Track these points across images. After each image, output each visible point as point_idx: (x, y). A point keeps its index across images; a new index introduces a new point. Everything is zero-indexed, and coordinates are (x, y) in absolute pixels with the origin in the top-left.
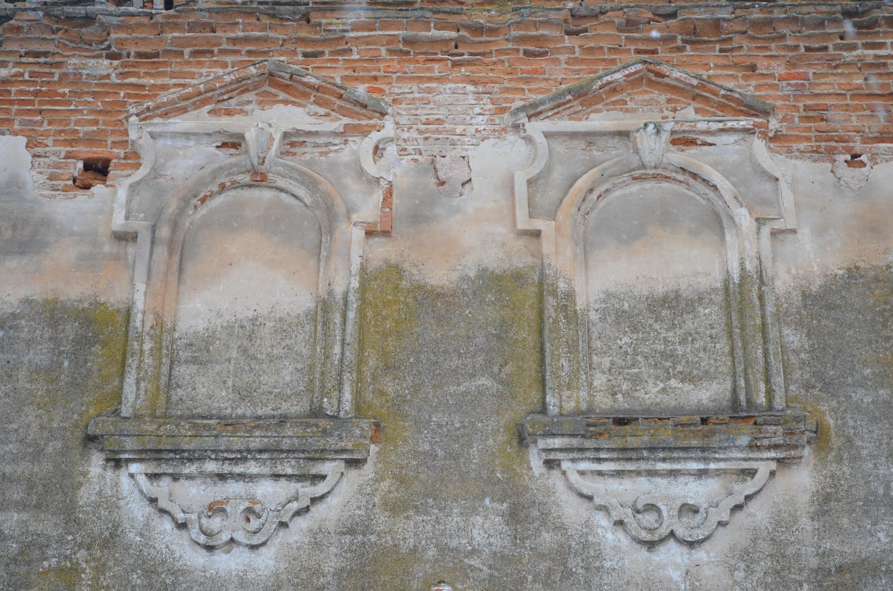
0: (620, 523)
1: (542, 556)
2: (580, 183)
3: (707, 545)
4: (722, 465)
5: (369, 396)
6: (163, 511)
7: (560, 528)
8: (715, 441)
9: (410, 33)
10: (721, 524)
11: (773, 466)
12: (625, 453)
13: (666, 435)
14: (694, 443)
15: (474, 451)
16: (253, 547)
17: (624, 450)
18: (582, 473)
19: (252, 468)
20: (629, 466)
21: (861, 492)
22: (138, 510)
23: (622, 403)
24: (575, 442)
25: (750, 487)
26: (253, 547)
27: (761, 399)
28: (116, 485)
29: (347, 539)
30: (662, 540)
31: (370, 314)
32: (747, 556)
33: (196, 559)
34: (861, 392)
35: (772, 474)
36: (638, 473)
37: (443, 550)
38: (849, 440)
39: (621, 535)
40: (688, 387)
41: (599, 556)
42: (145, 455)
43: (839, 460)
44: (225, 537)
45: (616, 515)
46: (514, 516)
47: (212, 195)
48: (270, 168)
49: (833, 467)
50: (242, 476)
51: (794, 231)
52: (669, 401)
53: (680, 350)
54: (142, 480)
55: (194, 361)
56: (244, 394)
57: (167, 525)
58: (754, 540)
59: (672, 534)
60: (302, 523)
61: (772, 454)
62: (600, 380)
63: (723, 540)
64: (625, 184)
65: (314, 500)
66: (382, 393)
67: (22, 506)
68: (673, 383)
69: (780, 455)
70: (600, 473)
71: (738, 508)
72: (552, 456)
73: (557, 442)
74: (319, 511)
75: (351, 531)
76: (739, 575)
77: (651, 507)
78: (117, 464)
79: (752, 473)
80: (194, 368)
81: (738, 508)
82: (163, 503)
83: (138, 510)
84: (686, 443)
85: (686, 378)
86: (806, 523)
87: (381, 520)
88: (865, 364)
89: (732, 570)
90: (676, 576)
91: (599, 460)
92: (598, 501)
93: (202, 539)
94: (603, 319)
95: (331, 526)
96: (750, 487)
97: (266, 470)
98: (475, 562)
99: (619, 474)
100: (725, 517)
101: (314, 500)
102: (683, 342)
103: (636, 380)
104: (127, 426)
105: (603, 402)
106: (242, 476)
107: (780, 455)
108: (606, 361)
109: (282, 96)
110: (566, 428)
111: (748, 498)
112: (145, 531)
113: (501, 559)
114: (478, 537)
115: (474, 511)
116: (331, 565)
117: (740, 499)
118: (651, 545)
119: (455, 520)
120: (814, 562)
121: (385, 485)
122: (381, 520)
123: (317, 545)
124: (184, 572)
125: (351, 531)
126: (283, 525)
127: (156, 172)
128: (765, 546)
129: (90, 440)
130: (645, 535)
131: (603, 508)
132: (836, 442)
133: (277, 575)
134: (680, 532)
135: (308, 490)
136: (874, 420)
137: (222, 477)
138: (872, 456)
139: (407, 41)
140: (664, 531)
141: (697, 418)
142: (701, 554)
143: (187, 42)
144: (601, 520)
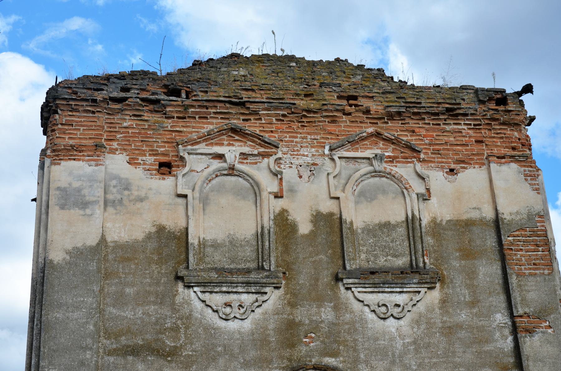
11: (426, 289)
12: (375, 285)
13: (389, 278)
18: (359, 292)
19: (240, 289)
20: (376, 290)
26: (242, 319)
29: (276, 317)
35: (426, 292)
36: (379, 292)
40: (395, 259)
44: (232, 316)
47: (213, 179)
50: (236, 292)
52: (388, 265)
56: (233, 260)
58: (420, 317)
73: (351, 281)
74: (265, 306)
75: (277, 314)
76: (415, 330)
83: (199, 305)
89: (413, 328)
90: (393, 330)
92: (365, 303)
96: (418, 297)
97: (244, 290)
98: (323, 325)
103: (376, 256)
105: (365, 265)
108: (365, 249)
120: (440, 325)
126: (253, 311)
131: (368, 306)
142: (401, 322)
143: (197, 113)
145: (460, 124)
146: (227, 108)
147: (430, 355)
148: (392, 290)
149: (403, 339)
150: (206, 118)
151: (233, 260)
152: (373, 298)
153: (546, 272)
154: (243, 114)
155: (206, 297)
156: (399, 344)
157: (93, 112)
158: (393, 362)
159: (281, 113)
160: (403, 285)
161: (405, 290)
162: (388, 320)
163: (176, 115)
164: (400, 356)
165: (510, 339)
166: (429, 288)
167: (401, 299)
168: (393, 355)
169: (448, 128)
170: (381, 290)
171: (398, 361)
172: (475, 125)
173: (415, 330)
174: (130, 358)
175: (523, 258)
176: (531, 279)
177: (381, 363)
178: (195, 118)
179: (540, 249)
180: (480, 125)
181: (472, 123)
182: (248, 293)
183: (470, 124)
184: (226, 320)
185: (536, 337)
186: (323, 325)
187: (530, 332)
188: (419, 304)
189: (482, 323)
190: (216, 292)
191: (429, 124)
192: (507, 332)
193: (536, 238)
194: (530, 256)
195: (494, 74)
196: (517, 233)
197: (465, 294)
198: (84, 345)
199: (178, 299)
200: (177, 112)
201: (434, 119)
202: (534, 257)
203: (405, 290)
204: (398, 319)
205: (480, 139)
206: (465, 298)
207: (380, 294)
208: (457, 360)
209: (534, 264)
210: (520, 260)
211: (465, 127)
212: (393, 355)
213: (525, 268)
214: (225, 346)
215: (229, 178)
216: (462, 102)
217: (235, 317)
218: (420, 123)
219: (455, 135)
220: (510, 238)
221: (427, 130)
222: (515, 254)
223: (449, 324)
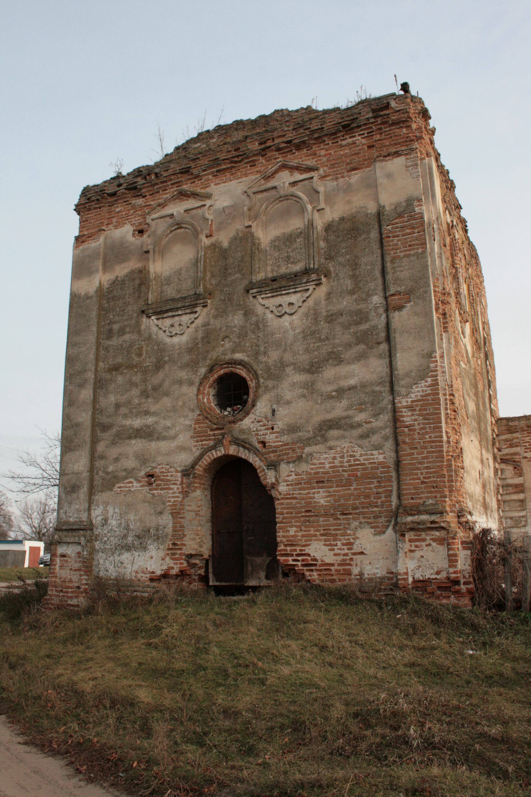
0: (272, 312)
1: (252, 324)
2: (263, 207)
3: (296, 314)
4: (300, 289)
5: (208, 286)
6: (160, 328)
7: (257, 316)
8: (297, 282)
9: (218, 169)
10: (300, 307)
11: (314, 286)
12: (272, 290)
13: (284, 283)
14: (291, 284)
15: (235, 297)
16: (181, 334)
17: (272, 289)
18: (262, 298)
19: (180, 312)
20: (275, 294)
21: (339, 290)
22: (154, 329)
23: (275, 274)
24: (259, 290)
25: (307, 294)
26: (181, 334)
27: (312, 266)
28: (149, 323)
29: (204, 328)
30: (283, 315)
31: (208, 261)
32: (306, 315)
33: (168, 340)
34: (341, 258)
35: (314, 289)
36: (277, 295)
37: (227, 327)
38: (337, 274)
39: (273, 315)
40: (293, 266)
41: (267, 322)
42: (156, 313)
43: (334, 281)
44: (174, 333)
45: (271, 309)
46: (246, 314)
47: (168, 234)
48: (392, 511)
49: (332, 283)
50: (178, 315)
51: (323, 209)
52: (288, 271)
53: (291, 254)
54: (155, 321)
55: (167, 284)
56: (179, 291)
57: (161, 332)
58: (309, 310)
59: (286, 312)
60: (193, 325)
61: (313, 283)
62: (269, 268)
63: (301, 311)
64: (277, 204)
65: (195, 319)
66: (211, 284)
67: (129, 333)
68: (289, 265)
69: (316, 282)
70: (268, 297)
71: (304, 301)
72: (254, 295)
73: (255, 291)
74: (197, 321)
75: (205, 326)
76: (304, 321)
77: (280, 305)
78: (150, 317)
79: (308, 290)
80: (167, 286)
81: (304, 301)
82: (160, 326)
83: (154, 329)
84: (288, 284)
85: (292, 263)
86: (323, 302)
87: (212, 321)
88: (343, 248)
89: (302, 320)
91: (266, 294)
92: (266, 306)
93: (169, 334)
94: (270, 249)
95: (200, 325)
96: (307, 294)
97: (183, 312)
98: (235, 329)
99: (273, 296)
100: (300, 305)
101: (195, 319)
102: (292, 251)
103: (279, 266)
104: (150, 307)
105: (270, 275)
106: (178, 315)
107: (316, 282)
108: (271, 262)
109: (185, 198)
110: (257, 286)
111: (307, 298)
112: (157, 334)
113: (242, 327)
114: (236, 322)
115: (235, 314)
116: (200, 336)
117: (305, 298)
118: (280, 316)
119: (230, 318)
120: (325, 314)
121: (212, 311)
122: (212, 321)
123: (197, 331)
124: (166, 344)
125: (205, 326)
126: (188, 327)
127: (154, 232)
128: (312, 312)
129: (143, 312)
130: (278, 314)
131: (267, 308)
132: (333, 275)
133: (187, 341)
134: (287, 311)
135: (193, 316)
136: (344, 266)
137: (174, 316)
138: (343, 278)
139: (217, 171)
140: (283, 312)
141: (293, 276)
142: (294, 317)
143: (159, 188)
144: (267, 311)
145: (355, 136)
146: (178, 178)
147: (315, 341)
148: (288, 291)
149: (295, 330)
150: (166, 190)
151: (179, 291)
152: (272, 302)
153: (420, 251)
154: (190, 179)
155: (160, 322)
156: (291, 335)
157: (100, 208)
158: (285, 350)
159: (215, 170)
160: (295, 286)
161: (297, 290)
162: (284, 317)
163: (147, 194)
164: (291, 345)
165: (384, 316)
166: (316, 285)
167: (293, 298)
168: (286, 344)
169: (344, 143)
170: (279, 293)
171: (288, 349)
172: (368, 133)
173: (304, 321)
174: (114, 373)
175: (399, 243)
176: (405, 260)
177: (276, 352)
178: (159, 192)
179: (416, 231)
180: (373, 132)
181: (366, 132)
182: (186, 314)
183: (364, 134)
184: (171, 336)
185: (405, 311)
186: (235, 329)
187: (400, 308)
188: (309, 299)
189: (361, 306)
190: (166, 318)
191: (328, 144)
192: (381, 310)
193: (413, 221)
194: (406, 239)
195: (395, 76)
196: (396, 221)
197: (349, 284)
198: (331, 295)
199: (143, 327)
200: (149, 191)
201: (334, 139)
202: (409, 240)
203: (297, 290)
204: (291, 314)
205: (371, 144)
206: (347, 287)
207: (279, 297)
208: (337, 341)
209: (410, 246)
210: (397, 244)
211: (359, 138)
212: (286, 344)
213: (401, 252)
214: (169, 356)
215: (179, 231)
216: (358, 116)
217: (176, 334)
218: (322, 145)
219: (350, 146)
220: (388, 227)
221: (327, 150)
222: (392, 241)
223: (332, 312)
